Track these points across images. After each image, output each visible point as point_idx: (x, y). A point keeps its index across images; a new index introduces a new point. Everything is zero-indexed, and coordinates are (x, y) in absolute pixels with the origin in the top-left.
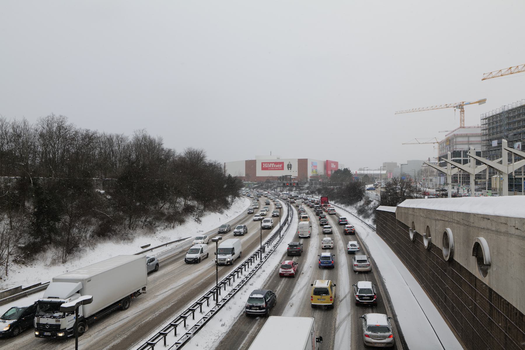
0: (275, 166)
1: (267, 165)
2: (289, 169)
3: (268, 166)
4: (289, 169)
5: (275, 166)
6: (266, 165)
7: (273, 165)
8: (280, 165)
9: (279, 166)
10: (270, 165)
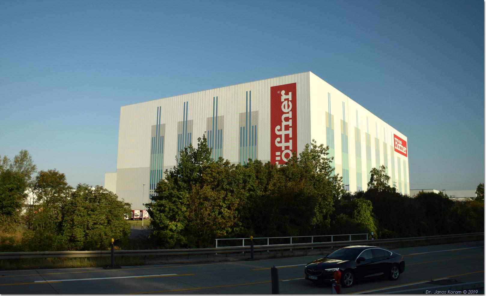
5: (287, 119)
8: (284, 97)
10: (283, 145)
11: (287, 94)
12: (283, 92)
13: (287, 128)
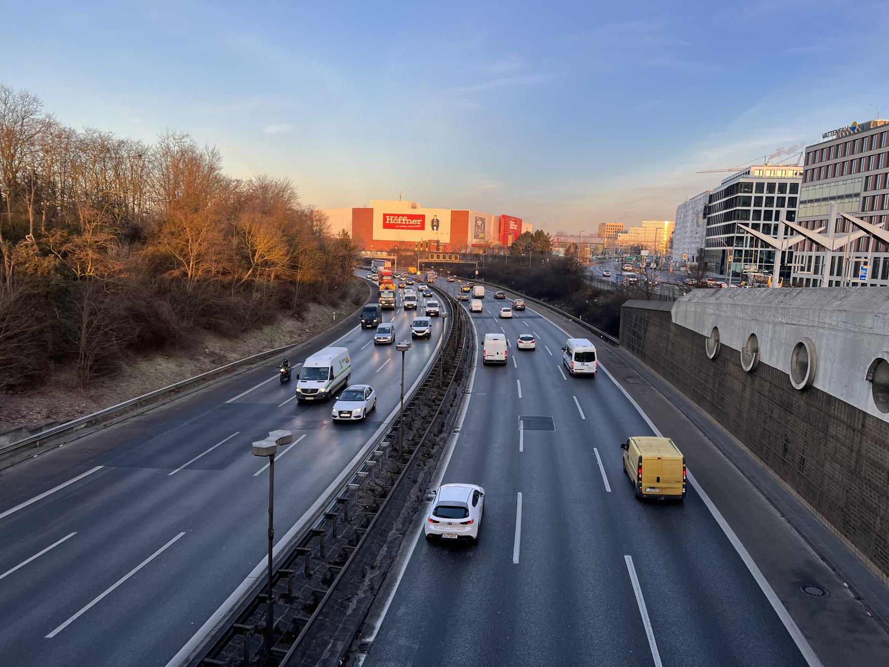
0: (409, 222)
1: (393, 219)
2: (435, 228)
3: (396, 221)
4: (435, 228)
6: (391, 219)
7: (404, 220)
8: (419, 221)
9: (416, 221)
10: (400, 220)
11: (420, 222)
12: (421, 221)
13: (406, 221)
